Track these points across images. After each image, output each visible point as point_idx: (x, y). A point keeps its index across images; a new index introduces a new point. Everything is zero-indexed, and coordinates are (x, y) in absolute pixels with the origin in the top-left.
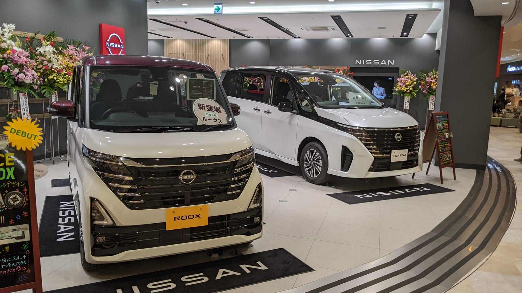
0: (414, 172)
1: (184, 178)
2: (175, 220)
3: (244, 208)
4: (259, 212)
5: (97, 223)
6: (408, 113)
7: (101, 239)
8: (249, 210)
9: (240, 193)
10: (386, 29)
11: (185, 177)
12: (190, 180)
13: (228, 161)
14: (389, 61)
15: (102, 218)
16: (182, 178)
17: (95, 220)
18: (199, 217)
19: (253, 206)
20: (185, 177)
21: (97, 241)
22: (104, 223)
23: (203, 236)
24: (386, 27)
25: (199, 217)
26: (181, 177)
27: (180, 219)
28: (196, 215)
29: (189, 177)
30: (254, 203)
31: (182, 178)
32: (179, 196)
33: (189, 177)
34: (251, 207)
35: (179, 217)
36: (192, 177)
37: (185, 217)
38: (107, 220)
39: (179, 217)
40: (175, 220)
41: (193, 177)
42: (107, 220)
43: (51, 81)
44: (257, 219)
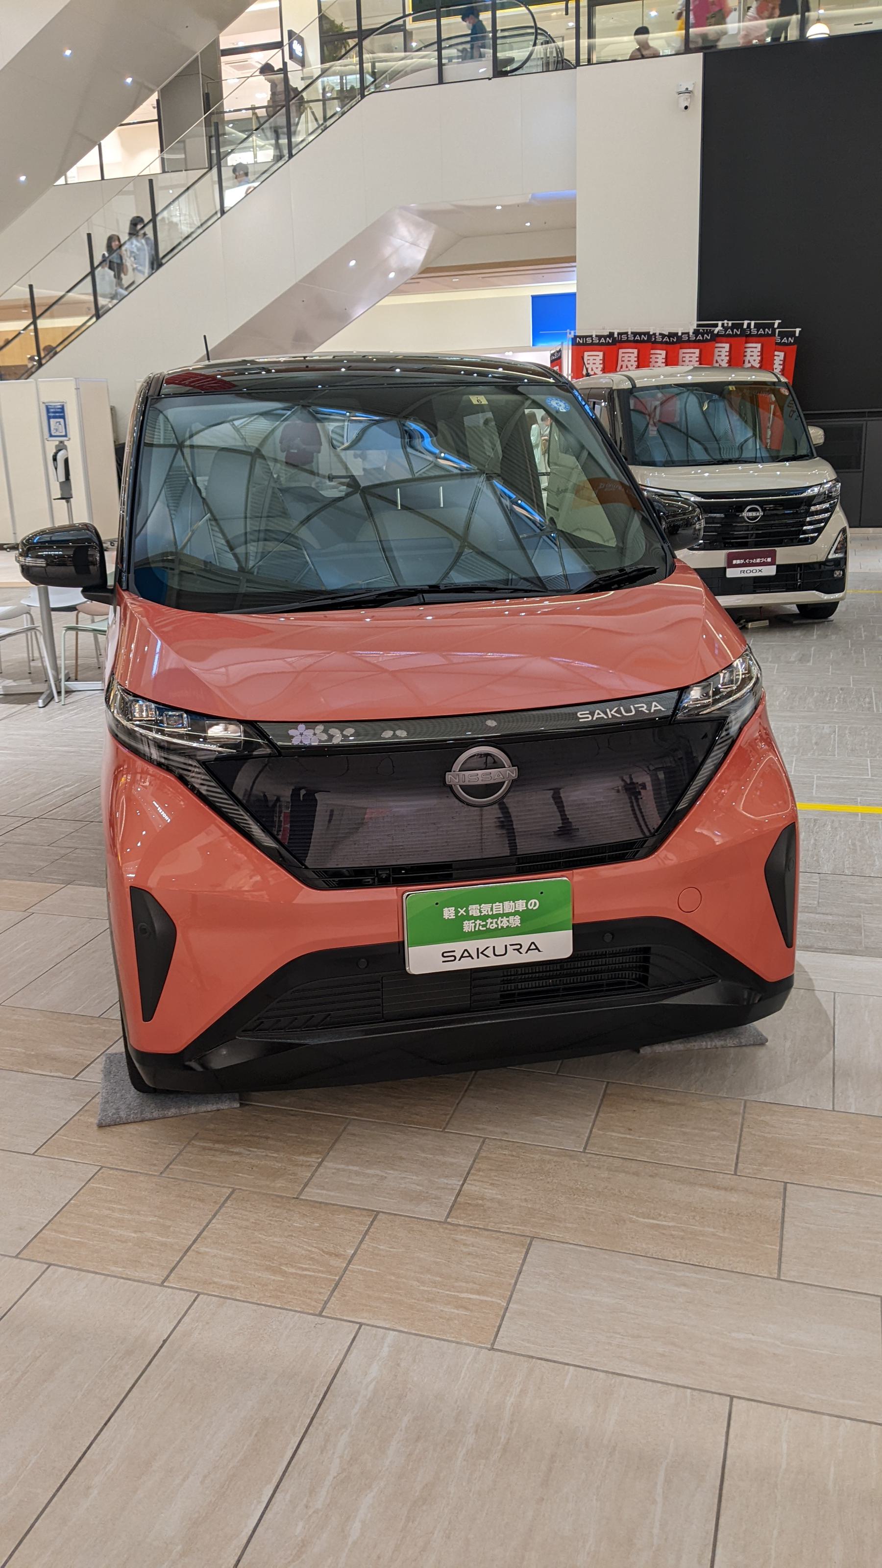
0: (225, 216)
3: (821, 558)
4: (840, 564)
9: (817, 537)
10: (118, 407)
11: (750, 514)
12: (756, 517)
13: (802, 495)
14: (735, 330)
20: (750, 514)
24: (109, 411)
29: (754, 514)
33: (754, 514)
34: (830, 557)
36: (758, 514)
43: (790, 725)
44: (838, 574)
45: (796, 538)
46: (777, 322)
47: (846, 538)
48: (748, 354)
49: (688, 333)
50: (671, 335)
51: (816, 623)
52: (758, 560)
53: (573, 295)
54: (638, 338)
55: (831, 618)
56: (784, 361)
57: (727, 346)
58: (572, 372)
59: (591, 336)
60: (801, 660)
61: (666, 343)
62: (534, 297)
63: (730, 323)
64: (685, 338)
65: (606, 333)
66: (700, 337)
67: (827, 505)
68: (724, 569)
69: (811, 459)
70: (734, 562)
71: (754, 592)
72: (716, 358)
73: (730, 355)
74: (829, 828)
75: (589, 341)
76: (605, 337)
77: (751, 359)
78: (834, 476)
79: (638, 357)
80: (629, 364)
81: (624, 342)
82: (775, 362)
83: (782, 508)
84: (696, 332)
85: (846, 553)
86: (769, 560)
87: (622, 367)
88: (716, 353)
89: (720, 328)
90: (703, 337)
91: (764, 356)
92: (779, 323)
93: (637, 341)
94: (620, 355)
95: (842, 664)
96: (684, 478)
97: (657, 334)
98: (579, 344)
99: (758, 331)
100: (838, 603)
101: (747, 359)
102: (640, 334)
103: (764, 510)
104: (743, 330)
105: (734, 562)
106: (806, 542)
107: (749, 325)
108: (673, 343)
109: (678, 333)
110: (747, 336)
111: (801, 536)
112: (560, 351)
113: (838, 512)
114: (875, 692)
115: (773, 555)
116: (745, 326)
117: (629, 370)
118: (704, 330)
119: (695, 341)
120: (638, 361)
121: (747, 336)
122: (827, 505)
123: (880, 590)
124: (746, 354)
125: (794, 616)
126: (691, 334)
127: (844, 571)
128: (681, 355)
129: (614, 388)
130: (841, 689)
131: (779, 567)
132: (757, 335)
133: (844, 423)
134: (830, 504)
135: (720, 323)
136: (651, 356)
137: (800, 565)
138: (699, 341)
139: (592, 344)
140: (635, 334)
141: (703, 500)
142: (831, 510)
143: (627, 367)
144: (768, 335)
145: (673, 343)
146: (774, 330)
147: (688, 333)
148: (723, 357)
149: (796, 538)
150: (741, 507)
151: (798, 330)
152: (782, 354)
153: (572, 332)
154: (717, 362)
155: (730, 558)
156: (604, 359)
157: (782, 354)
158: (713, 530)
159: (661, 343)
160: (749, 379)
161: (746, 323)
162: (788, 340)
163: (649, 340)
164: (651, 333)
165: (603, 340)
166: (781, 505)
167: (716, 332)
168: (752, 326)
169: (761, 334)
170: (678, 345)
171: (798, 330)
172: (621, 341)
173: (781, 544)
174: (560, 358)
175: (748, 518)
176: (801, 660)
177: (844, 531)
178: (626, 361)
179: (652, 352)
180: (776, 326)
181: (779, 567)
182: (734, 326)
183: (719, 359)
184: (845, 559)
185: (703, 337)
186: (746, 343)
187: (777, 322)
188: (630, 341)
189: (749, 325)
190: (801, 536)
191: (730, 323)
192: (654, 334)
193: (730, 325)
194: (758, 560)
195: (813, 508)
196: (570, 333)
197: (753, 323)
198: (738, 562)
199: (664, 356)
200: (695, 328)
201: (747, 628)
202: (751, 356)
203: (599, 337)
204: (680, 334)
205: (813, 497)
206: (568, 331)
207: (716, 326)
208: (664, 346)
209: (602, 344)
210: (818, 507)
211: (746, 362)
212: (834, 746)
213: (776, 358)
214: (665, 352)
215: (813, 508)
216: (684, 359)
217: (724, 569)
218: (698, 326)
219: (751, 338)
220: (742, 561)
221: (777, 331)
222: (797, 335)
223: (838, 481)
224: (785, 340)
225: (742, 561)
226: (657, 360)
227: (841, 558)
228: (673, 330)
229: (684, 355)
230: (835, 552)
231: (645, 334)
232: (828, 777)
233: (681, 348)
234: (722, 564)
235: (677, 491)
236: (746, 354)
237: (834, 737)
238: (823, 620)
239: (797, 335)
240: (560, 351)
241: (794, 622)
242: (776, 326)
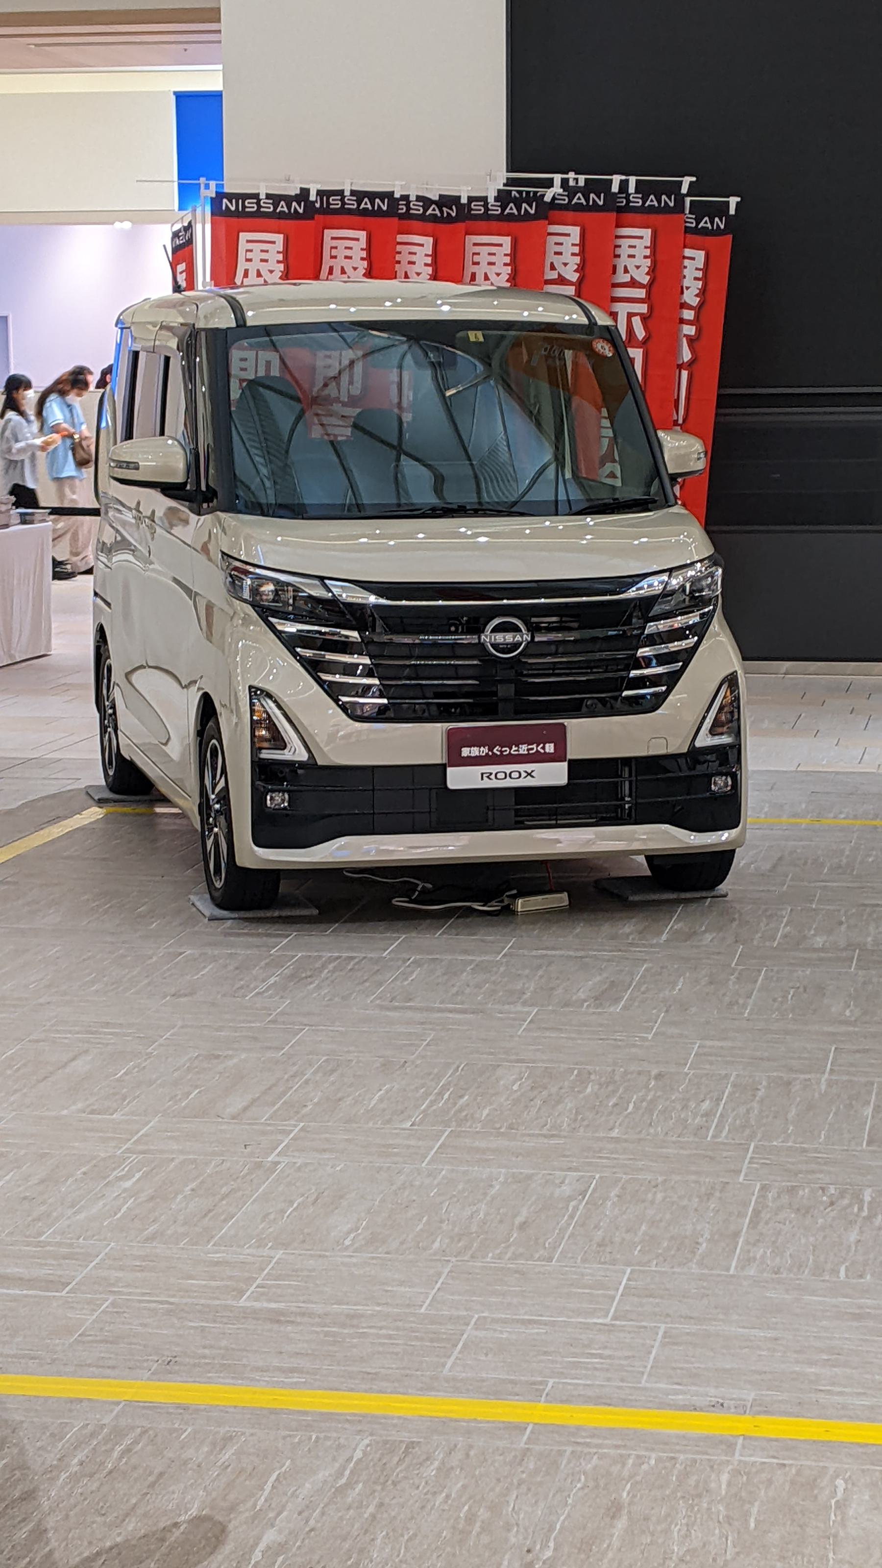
1: (495, 639)
2: (482, 779)
3: (677, 745)
5: (265, 755)
6: (571, 781)
7: (277, 800)
8: (695, 755)
11: (500, 638)
12: (516, 646)
15: (278, 741)
16: (491, 639)
17: (261, 749)
18: (533, 777)
19: (704, 740)
20: (500, 638)
21: (269, 802)
22: (286, 755)
23: (554, 822)
25: (533, 777)
26: (486, 636)
27: (493, 777)
28: (526, 772)
30: (712, 732)
31: (491, 639)
32: (561, 209)
35: (491, 774)
36: (518, 638)
37: (503, 775)
38: (293, 749)
39: (491, 774)
40: (482, 779)
41: (522, 637)
42: (293, 749)
44: (720, 784)
45: (615, 698)
46: (687, 181)
47: (737, 699)
48: (624, 251)
49: (484, 199)
50: (451, 201)
51: (679, 901)
52: (523, 749)
53: (217, 96)
54: (366, 204)
55: (722, 888)
56: (706, 269)
57: (575, 232)
58: (211, 279)
59: (256, 196)
60: (599, 998)
61: (434, 219)
62: (181, 97)
63: (582, 179)
64: (478, 209)
65: (294, 191)
66: (511, 209)
67: (694, 619)
68: (443, 767)
69: (662, 507)
70: (465, 752)
71: (519, 825)
72: (550, 258)
73: (582, 253)
74: (431, 1471)
75: (251, 206)
76: (288, 199)
77: (631, 264)
78: (707, 550)
79: (369, 249)
80: (348, 265)
81: (336, 212)
82: (686, 272)
83: (576, 625)
84: (503, 197)
85: (738, 734)
86: (550, 748)
87: (246, 274)
88: (551, 248)
89: (557, 189)
90: (519, 209)
91: (659, 257)
92: (691, 183)
93: (365, 213)
94: (328, 243)
95: (694, 1010)
96: (334, 548)
97: (413, 198)
98: (228, 213)
99: (503, 209)
100: (733, 851)
101: (621, 263)
102: (372, 196)
103: (534, 629)
104: (611, 198)
105: (465, 752)
106: (637, 706)
107: (624, 185)
108: (449, 220)
109: (459, 197)
110: (620, 210)
111: (626, 693)
112: (189, 228)
113: (718, 635)
114: (734, 1085)
115: (560, 737)
116: (615, 188)
117: (266, 283)
118: (520, 192)
119: (501, 218)
120: (369, 258)
121: (620, 210)
122: (694, 619)
123: (876, 817)
124: (618, 251)
125: (637, 883)
126: (491, 200)
127: (734, 777)
128: (470, 249)
129: (201, 325)
130: (659, 1077)
131: (574, 765)
132: (642, 210)
133: (843, 418)
134: (702, 616)
135: (557, 178)
136: (399, 248)
137: (627, 761)
138: (510, 218)
139: (258, 214)
140: (359, 195)
141: (383, 601)
142: (700, 630)
143: (259, 275)
144: (667, 209)
145: (449, 220)
146: (680, 200)
147: (484, 199)
148: (567, 257)
149: (615, 698)
150: (476, 620)
151: (733, 201)
152: (700, 255)
153: (213, 184)
154: (553, 268)
155: (454, 743)
156: (286, 252)
157: (700, 255)
158: (452, 672)
159: (422, 218)
160: (526, 316)
161: (617, 179)
162: (712, 223)
163: (392, 211)
164: (397, 195)
165: (283, 207)
166: (576, 617)
167: (548, 198)
168: (632, 189)
169: (511, 215)
170: (461, 226)
171: (733, 201)
172: (327, 211)
173: (576, 710)
174: (190, 242)
175: (494, 646)
176: (599, 998)
177: (731, 681)
178: (341, 257)
179: (400, 238)
180: (684, 190)
181: (574, 765)
182: (586, 191)
183: (557, 261)
184: (737, 748)
185: (519, 209)
186: (618, 226)
187: (687, 181)
188: (350, 212)
189: (624, 185)
190: (626, 693)
191: (582, 179)
192: (406, 198)
193: (581, 183)
194: (523, 749)
195: (651, 628)
196: (207, 187)
197: (632, 180)
198: (475, 751)
199: (429, 249)
200: (501, 187)
201: (514, 913)
202: (630, 256)
203: (276, 199)
204: (464, 200)
205: (648, 602)
206: (202, 180)
207: (549, 184)
208: (430, 226)
209: (282, 216)
210: (662, 626)
211: (620, 270)
212: (563, 1230)
213: (686, 262)
214: (431, 240)
215: (651, 628)
216: (476, 259)
217: (443, 767)
218: (510, 182)
219: (630, 216)
220: (484, 751)
221: (688, 200)
222: (732, 211)
223: (716, 564)
224: (705, 223)
225: (484, 751)
226: (413, 258)
227: (731, 746)
228: (450, 191)
229: (477, 249)
230: (712, 732)
231: (382, 196)
232: (505, 1321)
233: (468, 233)
234: (437, 757)
235: (322, 579)
236: (618, 251)
237: (576, 1208)
238: (704, 894)
239: (732, 211)
240: (189, 228)
241: (631, 898)
242: (684, 190)
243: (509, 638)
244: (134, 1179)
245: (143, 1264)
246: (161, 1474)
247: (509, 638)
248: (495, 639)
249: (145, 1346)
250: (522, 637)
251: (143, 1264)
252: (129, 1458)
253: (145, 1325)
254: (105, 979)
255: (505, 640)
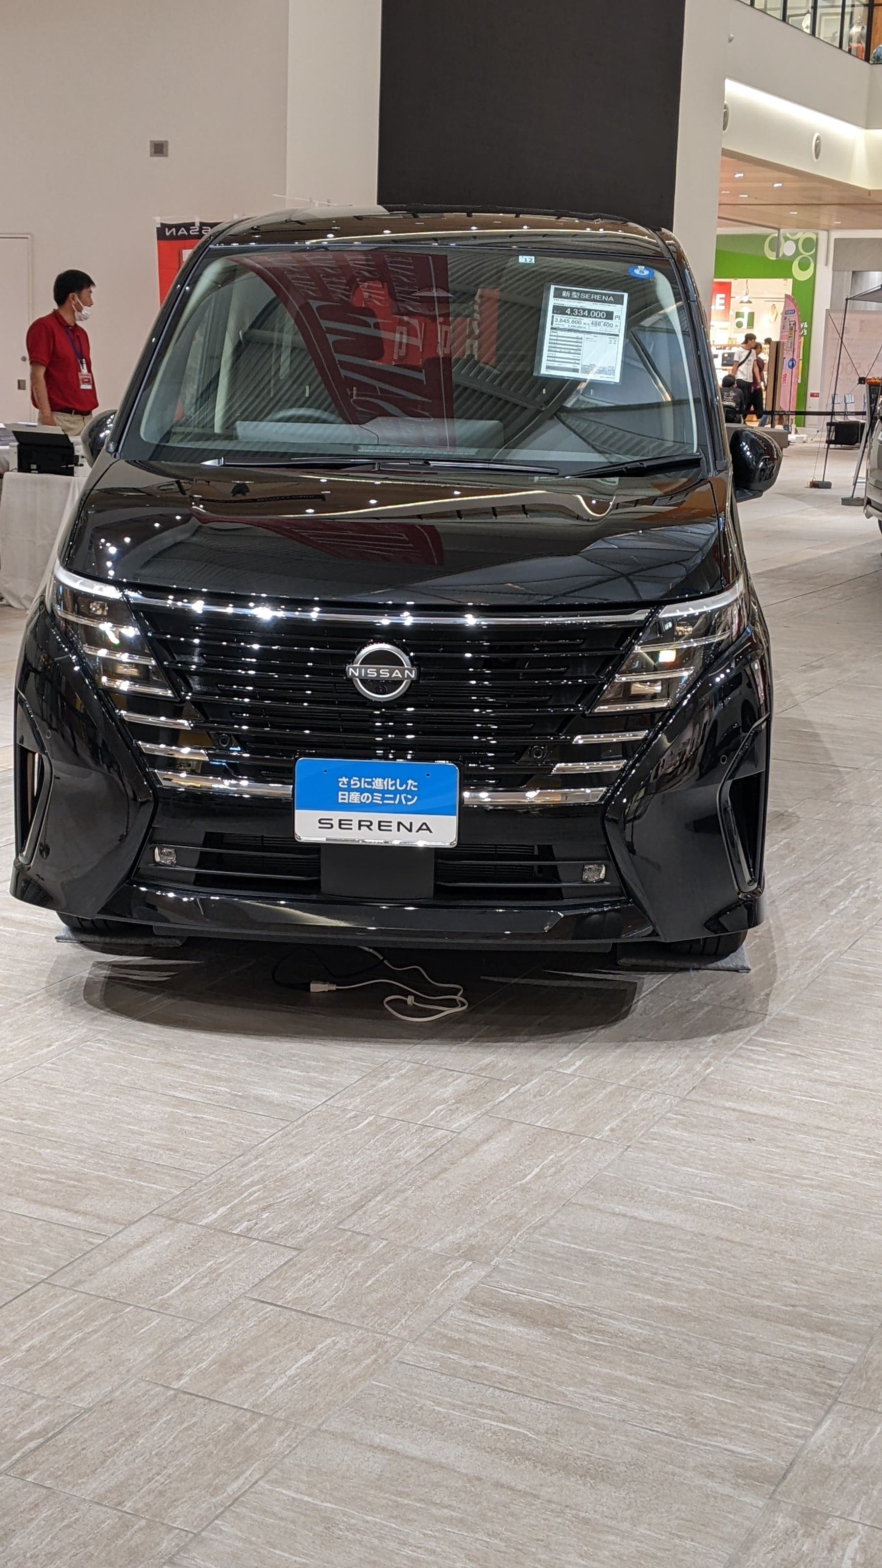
1: (366, 673)
11: (372, 672)
20: (372, 672)
26: (355, 669)
36: (397, 674)
41: (403, 674)
243: (385, 673)
244: (574, 1067)
245: (649, 1141)
246: (89, 1374)
247: (385, 673)
248: (366, 673)
249: (855, 1196)
250: (403, 674)
251: (649, 1141)
252: (75, 1350)
253: (855, 1175)
254: (870, 836)
255: (379, 674)
